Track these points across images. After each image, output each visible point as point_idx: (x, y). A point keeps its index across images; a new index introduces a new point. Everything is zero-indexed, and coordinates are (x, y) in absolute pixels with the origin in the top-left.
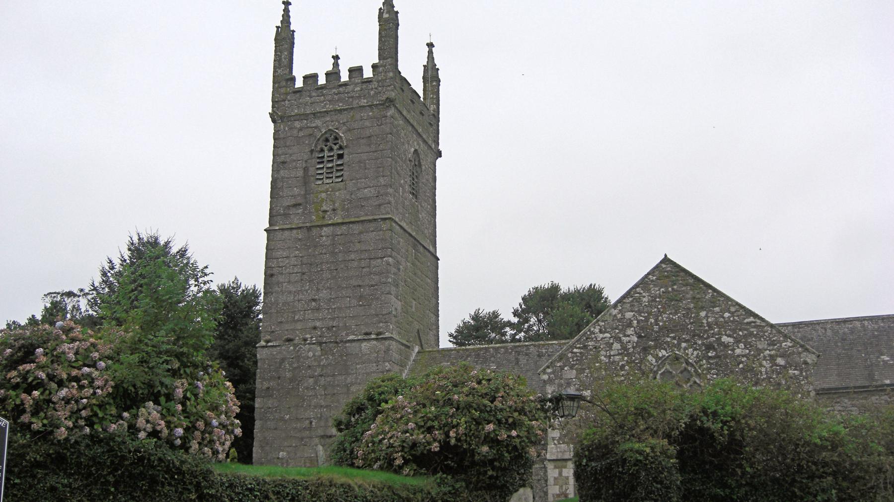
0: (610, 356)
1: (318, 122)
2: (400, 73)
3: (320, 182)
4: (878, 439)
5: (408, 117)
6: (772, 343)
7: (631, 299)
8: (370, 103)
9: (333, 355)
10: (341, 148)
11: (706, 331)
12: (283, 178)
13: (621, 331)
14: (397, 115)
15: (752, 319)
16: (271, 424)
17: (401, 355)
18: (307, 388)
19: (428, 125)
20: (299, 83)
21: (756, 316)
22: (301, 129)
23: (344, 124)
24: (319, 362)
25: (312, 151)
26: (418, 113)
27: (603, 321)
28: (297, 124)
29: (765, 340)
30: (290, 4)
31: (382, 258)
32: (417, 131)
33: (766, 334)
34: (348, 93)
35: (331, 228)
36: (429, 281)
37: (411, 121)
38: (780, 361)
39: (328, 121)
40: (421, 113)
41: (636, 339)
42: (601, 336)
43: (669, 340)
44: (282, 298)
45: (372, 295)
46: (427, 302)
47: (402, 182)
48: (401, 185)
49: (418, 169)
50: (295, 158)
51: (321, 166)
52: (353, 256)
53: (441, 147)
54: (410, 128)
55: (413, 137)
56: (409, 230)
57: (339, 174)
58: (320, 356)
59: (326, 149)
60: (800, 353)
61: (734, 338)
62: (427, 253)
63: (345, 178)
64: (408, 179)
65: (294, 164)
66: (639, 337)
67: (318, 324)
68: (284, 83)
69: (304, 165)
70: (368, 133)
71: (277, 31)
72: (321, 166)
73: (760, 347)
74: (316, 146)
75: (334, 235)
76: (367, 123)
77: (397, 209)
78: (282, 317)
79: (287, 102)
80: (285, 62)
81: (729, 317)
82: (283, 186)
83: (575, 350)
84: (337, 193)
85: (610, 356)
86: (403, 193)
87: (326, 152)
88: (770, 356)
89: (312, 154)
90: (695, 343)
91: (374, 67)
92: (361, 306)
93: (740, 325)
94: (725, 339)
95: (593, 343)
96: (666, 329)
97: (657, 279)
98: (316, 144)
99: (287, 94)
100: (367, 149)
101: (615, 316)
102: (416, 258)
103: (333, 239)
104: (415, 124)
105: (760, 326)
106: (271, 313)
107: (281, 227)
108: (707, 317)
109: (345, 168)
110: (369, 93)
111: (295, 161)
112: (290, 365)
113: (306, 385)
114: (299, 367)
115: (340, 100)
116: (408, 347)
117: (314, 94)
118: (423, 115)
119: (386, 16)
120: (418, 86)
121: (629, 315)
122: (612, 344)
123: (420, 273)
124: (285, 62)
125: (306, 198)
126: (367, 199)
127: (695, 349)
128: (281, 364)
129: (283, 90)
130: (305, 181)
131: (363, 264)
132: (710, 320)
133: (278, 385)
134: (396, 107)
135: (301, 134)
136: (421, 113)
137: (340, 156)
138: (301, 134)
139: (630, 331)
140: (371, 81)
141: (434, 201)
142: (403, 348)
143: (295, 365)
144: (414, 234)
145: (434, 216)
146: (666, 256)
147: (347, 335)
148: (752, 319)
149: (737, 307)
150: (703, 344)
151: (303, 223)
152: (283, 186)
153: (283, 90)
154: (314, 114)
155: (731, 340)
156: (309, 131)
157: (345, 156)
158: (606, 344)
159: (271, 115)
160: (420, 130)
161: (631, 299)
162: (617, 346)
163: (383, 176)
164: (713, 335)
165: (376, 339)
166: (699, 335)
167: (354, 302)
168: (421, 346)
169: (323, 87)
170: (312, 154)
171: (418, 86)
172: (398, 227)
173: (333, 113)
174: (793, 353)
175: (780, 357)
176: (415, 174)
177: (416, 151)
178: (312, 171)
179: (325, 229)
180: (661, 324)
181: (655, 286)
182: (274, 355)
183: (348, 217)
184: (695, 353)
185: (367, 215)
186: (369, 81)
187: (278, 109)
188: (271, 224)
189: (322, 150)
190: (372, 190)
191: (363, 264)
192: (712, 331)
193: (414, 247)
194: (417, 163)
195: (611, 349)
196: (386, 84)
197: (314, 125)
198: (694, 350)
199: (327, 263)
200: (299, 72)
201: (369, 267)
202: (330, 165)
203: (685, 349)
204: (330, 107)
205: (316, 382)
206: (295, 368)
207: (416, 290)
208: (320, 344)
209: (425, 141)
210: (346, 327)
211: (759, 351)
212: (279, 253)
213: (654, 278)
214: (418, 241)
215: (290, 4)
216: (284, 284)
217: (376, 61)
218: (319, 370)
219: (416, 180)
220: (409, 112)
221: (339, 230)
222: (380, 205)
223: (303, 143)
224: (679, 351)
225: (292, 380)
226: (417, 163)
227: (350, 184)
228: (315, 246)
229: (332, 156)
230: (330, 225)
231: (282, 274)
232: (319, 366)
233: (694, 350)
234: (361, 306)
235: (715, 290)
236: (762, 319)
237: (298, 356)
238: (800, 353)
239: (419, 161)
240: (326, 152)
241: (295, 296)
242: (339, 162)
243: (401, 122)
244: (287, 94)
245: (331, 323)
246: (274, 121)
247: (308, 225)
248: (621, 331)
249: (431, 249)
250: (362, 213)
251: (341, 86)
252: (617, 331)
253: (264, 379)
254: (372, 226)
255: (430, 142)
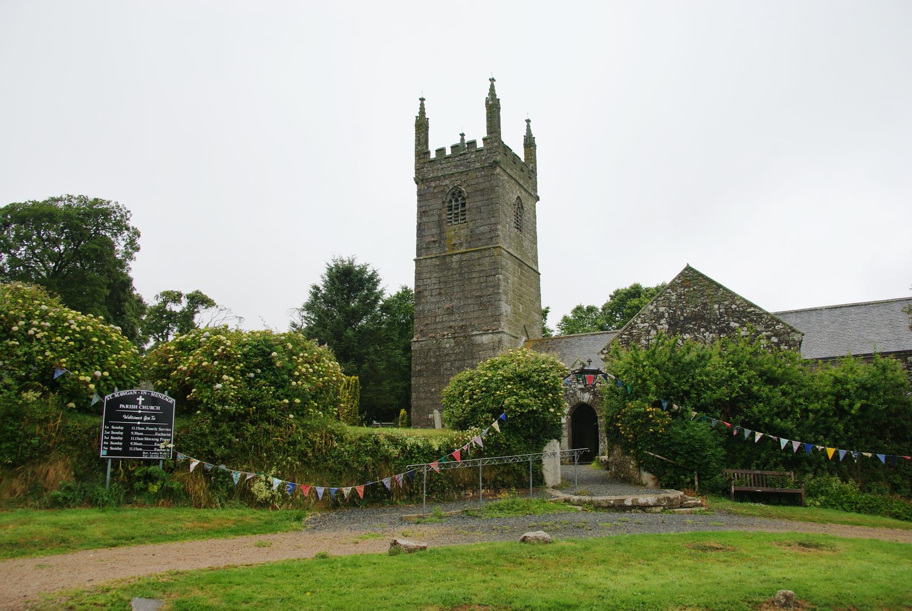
0: (648, 340)
1: (447, 182)
2: (503, 142)
3: (450, 224)
4: (728, 396)
5: (511, 173)
6: (767, 327)
7: (663, 297)
8: (482, 166)
9: (463, 345)
10: (464, 199)
11: (719, 319)
12: (424, 222)
13: (656, 321)
14: (502, 173)
15: (752, 309)
16: (423, 396)
17: (511, 343)
18: (446, 369)
19: (528, 178)
20: (433, 155)
21: (755, 306)
22: (435, 188)
23: (465, 181)
24: (454, 351)
25: (444, 202)
26: (519, 170)
27: (643, 315)
28: (433, 184)
29: (763, 324)
30: (425, 100)
31: (494, 275)
32: (519, 183)
33: (763, 319)
34: (467, 159)
35: (459, 256)
36: (533, 290)
37: (514, 176)
38: (774, 339)
39: (454, 180)
40: (522, 170)
41: (667, 326)
42: (642, 325)
43: (691, 326)
44: (427, 307)
45: (489, 302)
46: (531, 305)
47: (508, 220)
48: (507, 223)
49: (522, 211)
50: (432, 208)
51: (450, 212)
52: (474, 275)
53: (538, 194)
54: (513, 181)
55: (516, 188)
56: (515, 255)
57: (463, 217)
58: (454, 347)
59: (453, 200)
60: (789, 333)
61: (739, 323)
62: (531, 270)
63: (467, 220)
64: (513, 218)
65: (432, 212)
66: (670, 325)
67: (452, 324)
68: (422, 156)
69: (439, 212)
70: (481, 187)
71: (417, 119)
72: (450, 212)
73: (759, 329)
74: (446, 199)
75: (461, 261)
76: (481, 180)
77: (505, 240)
78: (427, 320)
79: (425, 169)
80: (422, 140)
81: (735, 308)
82: (424, 229)
83: (624, 336)
84: (462, 231)
85: (648, 340)
86: (509, 228)
87: (453, 202)
88: (766, 336)
89: (444, 204)
90: (711, 328)
91: (484, 140)
92: (481, 310)
93: (744, 314)
94: (733, 324)
95: (636, 331)
96: (688, 320)
97: (682, 282)
98: (446, 198)
99: (425, 163)
100: (481, 198)
101: (652, 310)
102: (521, 274)
103: (461, 264)
104: (517, 178)
105: (759, 314)
106: (420, 318)
107: (425, 257)
108: (719, 308)
109: (467, 213)
110: (481, 159)
111: (432, 210)
112: (435, 354)
113: (445, 367)
114: (440, 355)
115: (462, 165)
116: (517, 338)
117: (443, 162)
118: (523, 171)
119: (490, 102)
120: (519, 150)
121: (662, 309)
122: (650, 331)
123: (525, 285)
124: (422, 140)
125: (440, 236)
126: (483, 233)
127: (711, 333)
128: (427, 353)
129: (422, 161)
130: (440, 224)
131: (482, 280)
132: (721, 311)
133: (427, 368)
134: (501, 167)
135: (436, 191)
136: (522, 170)
137: (463, 205)
138: (436, 191)
139: (663, 321)
140: (482, 150)
141: (535, 233)
142: (512, 338)
143: (437, 354)
144: (519, 257)
145: (536, 243)
146: (688, 264)
147: (472, 331)
148: (752, 309)
149: (741, 300)
150: (716, 328)
151: (440, 253)
152: (424, 229)
153: (422, 161)
154: (444, 176)
155: (737, 325)
156: (441, 189)
157: (467, 205)
158: (646, 331)
159: (415, 179)
160: (521, 182)
161: (663, 297)
162: (653, 332)
163: (493, 217)
164: (724, 321)
165: (492, 333)
166: (713, 322)
167: (476, 307)
168: (528, 336)
169: (449, 157)
170: (444, 204)
171: (519, 150)
172: (505, 253)
173: (457, 174)
174: (784, 333)
175: (774, 336)
176: (519, 214)
177: (518, 198)
178: (444, 216)
179: (455, 257)
180: (685, 315)
181: (681, 287)
182: (423, 347)
183: (470, 248)
184: (711, 335)
185: (483, 245)
186: (481, 150)
187: (419, 174)
188: (418, 256)
189: (451, 201)
190: (486, 227)
191: (482, 280)
192: (723, 319)
193: (520, 266)
194: (520, 206)
195: (649, 334)
196: (493, 151)
197: (444, 184)
198: (710, 333)
199: (457, 281)
200: (433, 148)
201: (486, 282)
202: (456, 212)
203: (703, 333)
204: (454, 171)
205: (451, 365)
206: (438, 356)
207: (522, 297)
208: (454, 338)
209: (526, 190)
210: (472, 326)
211: (758, 333)
212: (424, 275)
213: (680, 281)
214: (523, 262)
215: (425, 100)
216: (428, 297)
217: (485, 135)
218: (453, 357)
219: (520, 218)
220: (511, 169)
221: (465, 257)
222: (491, 238)
223: (438, 197)
224: (699, 334)
225: (436, 364)
226: (520, 206)
227: (471, 224)
228: (448, 270)
229: (458, 205)
230: (458, 254)
231: (426, 290)
232: (453, 353)
233: (710, 333)
234: (481, 310)
235: (725, 289)
236: (760, 309)
237: (439, 347)
238: (789, 333)
239: (522, 205)
240: (453, 202)
241: (436, 305)
242: (463, 209)
243: (506, 178)
244: (425, 163)
245: (461, 324)
246: (417, 183)
247: (442, 254)
248: (656, 321)
249: (534, 267)
250: (480, 244)
251: (446, 158)
252: (654, 321)
253: (416, 364)
254: (487, 253)
255: (530, 191)
